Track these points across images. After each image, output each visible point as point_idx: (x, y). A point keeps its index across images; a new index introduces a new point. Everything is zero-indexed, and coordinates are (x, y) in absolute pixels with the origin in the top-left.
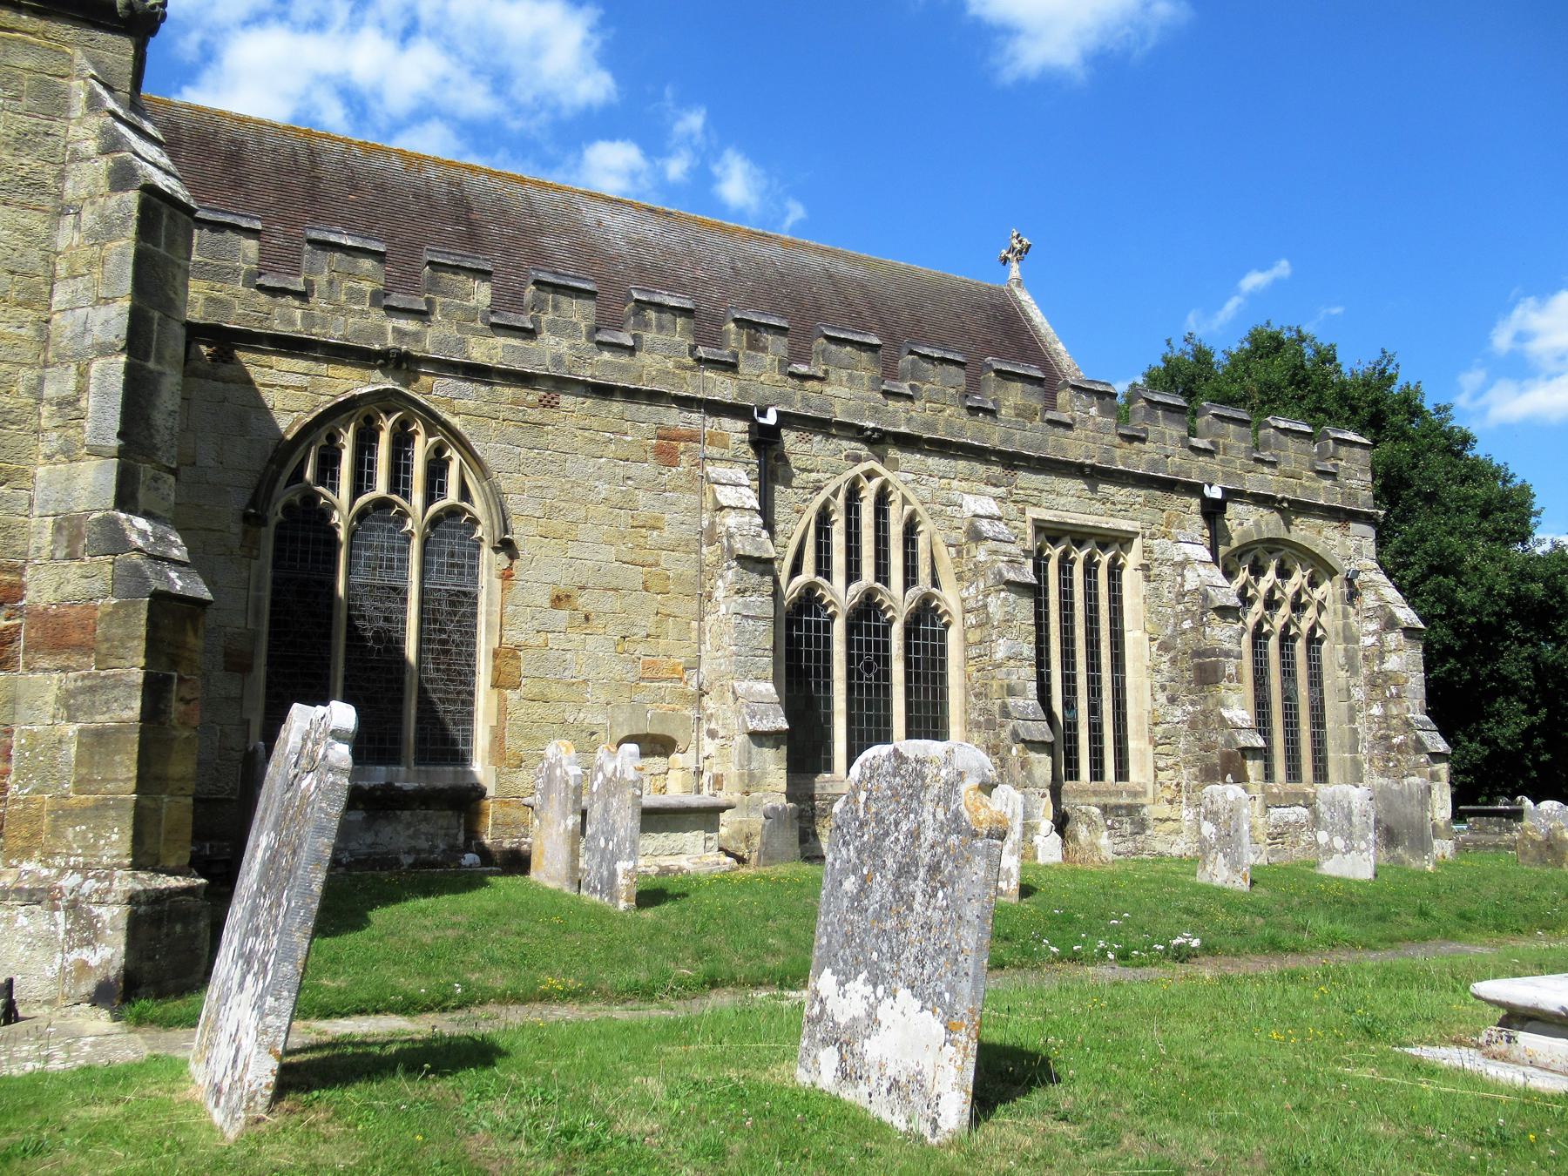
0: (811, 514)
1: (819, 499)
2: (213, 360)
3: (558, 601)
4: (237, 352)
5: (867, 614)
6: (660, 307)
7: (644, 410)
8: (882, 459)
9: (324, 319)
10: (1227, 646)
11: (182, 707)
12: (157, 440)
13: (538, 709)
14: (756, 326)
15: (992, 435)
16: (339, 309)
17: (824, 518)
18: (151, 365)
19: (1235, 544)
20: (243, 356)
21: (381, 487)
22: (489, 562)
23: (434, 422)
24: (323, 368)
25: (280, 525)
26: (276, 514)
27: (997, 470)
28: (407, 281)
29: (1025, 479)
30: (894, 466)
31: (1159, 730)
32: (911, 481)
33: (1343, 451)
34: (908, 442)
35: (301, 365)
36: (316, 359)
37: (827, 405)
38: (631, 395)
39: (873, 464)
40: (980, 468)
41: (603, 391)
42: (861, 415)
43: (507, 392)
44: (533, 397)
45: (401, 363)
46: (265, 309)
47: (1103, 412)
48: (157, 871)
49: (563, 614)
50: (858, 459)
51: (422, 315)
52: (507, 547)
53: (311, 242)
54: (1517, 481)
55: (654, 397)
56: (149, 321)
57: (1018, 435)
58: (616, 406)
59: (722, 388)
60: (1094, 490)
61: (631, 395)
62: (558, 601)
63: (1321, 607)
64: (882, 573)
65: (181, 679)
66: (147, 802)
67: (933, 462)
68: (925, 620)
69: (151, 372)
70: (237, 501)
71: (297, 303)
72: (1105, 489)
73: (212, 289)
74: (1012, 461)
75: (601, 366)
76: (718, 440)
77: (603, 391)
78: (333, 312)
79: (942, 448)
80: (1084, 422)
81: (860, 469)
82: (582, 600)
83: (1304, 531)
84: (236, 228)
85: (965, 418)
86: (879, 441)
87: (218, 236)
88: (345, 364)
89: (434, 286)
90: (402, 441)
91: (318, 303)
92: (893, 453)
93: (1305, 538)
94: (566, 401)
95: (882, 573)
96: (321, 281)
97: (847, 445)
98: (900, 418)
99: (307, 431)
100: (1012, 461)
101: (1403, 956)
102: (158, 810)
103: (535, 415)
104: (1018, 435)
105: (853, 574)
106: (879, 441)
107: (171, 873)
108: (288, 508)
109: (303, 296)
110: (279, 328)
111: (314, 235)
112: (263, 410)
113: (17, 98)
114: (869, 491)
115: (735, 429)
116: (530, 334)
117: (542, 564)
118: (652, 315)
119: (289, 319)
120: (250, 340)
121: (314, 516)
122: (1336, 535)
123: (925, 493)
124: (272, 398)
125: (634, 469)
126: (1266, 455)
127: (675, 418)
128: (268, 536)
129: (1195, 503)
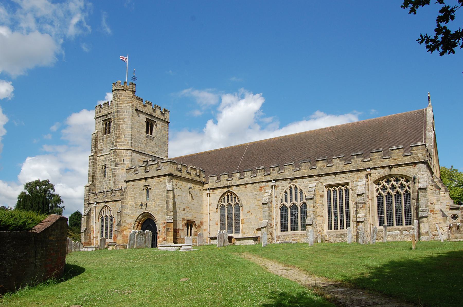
7: (257, 184)
15: (315, 172)
21: (294, 201)
28: (254, 173)
29: (323, 178)
32: (300, 184)
33: (414, 148)
34: (322, 175)
37: (417, 158)
42: (290, 176)
43: (241, 187)
45: (228, 187)
50: (290, 183)
54: (61, 205)
55: (258, 182)
64: (296, 200)
67: (304, 180)
79: (305, 177)
86: (292, 180)
90: (231, 195)
95: (296, 200)
98: (298, 174)
103: (245, 189)
105: (291, 200)
122: (412, 169)
125: (257, 193)
127: (262, 184)
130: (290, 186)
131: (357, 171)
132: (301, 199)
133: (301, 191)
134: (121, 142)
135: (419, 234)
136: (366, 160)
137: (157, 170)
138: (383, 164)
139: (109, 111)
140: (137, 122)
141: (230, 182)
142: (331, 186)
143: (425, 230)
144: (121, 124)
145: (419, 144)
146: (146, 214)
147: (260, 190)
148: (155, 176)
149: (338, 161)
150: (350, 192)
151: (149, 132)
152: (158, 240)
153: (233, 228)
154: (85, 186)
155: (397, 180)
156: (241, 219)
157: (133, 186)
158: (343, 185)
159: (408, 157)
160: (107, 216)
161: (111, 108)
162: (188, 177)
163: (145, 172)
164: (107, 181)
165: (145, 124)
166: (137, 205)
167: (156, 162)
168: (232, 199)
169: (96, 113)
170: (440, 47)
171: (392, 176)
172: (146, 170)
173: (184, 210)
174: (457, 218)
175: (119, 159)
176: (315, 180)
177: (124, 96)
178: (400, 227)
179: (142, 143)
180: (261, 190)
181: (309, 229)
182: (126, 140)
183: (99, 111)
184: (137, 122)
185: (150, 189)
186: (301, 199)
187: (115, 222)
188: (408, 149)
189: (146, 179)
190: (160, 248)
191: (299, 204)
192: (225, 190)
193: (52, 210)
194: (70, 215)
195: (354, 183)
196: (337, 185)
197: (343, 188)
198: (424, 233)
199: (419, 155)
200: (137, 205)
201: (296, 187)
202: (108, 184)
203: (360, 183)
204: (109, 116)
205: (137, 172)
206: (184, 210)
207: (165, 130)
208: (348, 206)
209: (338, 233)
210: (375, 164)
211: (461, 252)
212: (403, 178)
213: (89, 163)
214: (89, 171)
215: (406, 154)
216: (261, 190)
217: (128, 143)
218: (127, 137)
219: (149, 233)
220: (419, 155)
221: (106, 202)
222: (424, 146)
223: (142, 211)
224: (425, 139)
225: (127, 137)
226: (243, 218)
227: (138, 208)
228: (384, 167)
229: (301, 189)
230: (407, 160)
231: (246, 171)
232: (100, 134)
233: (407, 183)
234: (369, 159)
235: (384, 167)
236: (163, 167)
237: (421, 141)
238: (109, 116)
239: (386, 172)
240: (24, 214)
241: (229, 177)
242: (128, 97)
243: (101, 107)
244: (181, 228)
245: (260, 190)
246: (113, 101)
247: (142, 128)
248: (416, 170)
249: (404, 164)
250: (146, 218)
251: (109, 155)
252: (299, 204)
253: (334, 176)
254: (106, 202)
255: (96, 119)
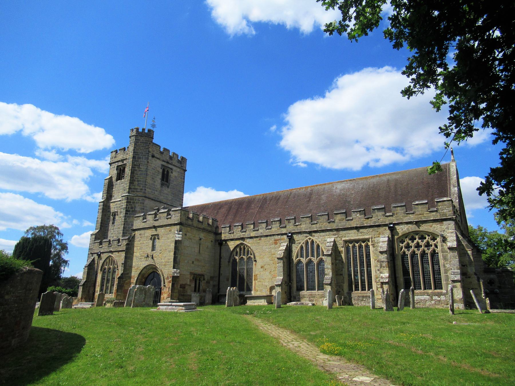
0: (299, 248)
1: (300, 245)
3: (262, 267)
5: (423, 254)
6: (275, 221)
7: (272, 237)
8: (311, 236)
10: (383, 260)
13: (260, 283)
14: (289, 219)
15: (334, 226)
17: (302, 247)
19: (400, 235)
22: (254, 263)
23: (247, 246)
27: (335, 232)
29: (342, 233)
30: (314, 236)
31: (378, 279)
32: (317, 238)
33: (439, 204)
35: (233, 242)
38: (270, 235)
39: (310, 237)
40: (331, 233)
41: (267, 236)
44: (258, 239)
45: (243, 239)
47: (360, 215)
49: (262, 269)
50: (307, 237)
51: (245, 232)
52: (255, 261)
55: (273, 235)
57: (340, 224)
58: (269, 238)
59: (284, 231)
60: (358, 231)
61: (270, 235)
62: (262, 267)
63: (436, 246)
67: (322, 234)
68: (434, 254)
70: (227, 260)
72: (361, 230)
74: (338, 230)
75: (267, 232)
76: (284, 239)
77: (267, 236)
79: (323, 231)
80: (355, 218)
81: (307, 238)
82: (265, 267)
83: (424, 228)
85: (328, 224)
86: (310, 233)
89: (247, 227)
90: (244, 249)
91: (235, 233)
92: (313, 234)
93: (425, 229)
94: (262, 238)
97: (305, 235)
98: (315, 228)
99: (233, 250)
100: (338, 230)
103: (259, 241)
104: (340, 224)
105: (307, 256)
106: (310, 233)
109: (233, 233)
114: (309, 241)
115: (285, 236)
116: (258, 230)
117: (260, 262)
118: (274, 223)
119: (232, 236)
120: (228, 240)
121: (235, 260)
123: (320, 240)
126: (331, 220)
127: (277, 237)
129: (387, 228)
130: (307, 240)
131: (379, 226)
132: (318, 255)
133: (318, 246)
135: (453, 301)
136: (388, 214)
137: (167, 219)
138: (406, 220)
139: (125, 157)
140: (153, 169)
141: (244, 233)
142: (351, 241)
143: (458, 296)
144: (136, 170)
145: (445, 199)
147: (275, 243)
149: (358, 215)
150: (371, 249)
151: (165, 180)
152: (162, 296)
155: (422, 238)
156: (254, 274)
157: (140, 235)
158: (364, 241)
159: (434, 213)
160: (110, 269)
161: (127, 154)
162: (200, 226)
165: (161, 171)
166: (142, 256)
167: (166, 210)
168: (244, 252)
170: (481, 117)
171: (416, 233)
173: (193, 262)
174: (493, 283)
175: (130, 206)
176: (333, 235)
178: (430, 291)
179: (156, 191)
180: (276, 243)
181: (327, 289)
182: (140, 186)
184: (153, 169)
186: (318, 255)
187: (118, 275)
188: (431, 205)
189: (155, 227)
190: (161, 307)
191: (315, 260)
192: (238, 242)
194: (15, 243)
195: (376, 239)
196: (357, 241)
197: (363, 244)
198: (458, 299)
199: (445, 211)
200: (142, 256)
201: (312, 242)
202: (116, 232)
203: (381, 239)
204: (125, 162)
205: (145, 220)
206: (193, 262)
207: (181, 178)
208: (369, 265)
209: (360, 295)
210: (398, 219)
211: (3, 101)
212: (429, 236)
213: (99, 209)
215: (431, 209)
216: (276, 243)
220: (445, 211)
221: (111, 252)
222: (450, 202)
223: (147, 263)
224: (450, 195)
226: (256, 273)
228: (407, 223)
229: (318, 244)
230: (433, 216)
231: (261, 223)
232: (114, 179)
233: (434, 241)
234: (391, 214)
235: (407, 223)
237: (447, 196)
238: (125, 162)
239: (413, 228)
240: (19, 262)
242: (146, 143)
244: (188, 283)
245: (275, 243)
248: (443, 227)
249: (430, 220)
250: (151, 271)
251: (120, 202)
252: (315, 260)
253: (355, 231)
254: (111, 252)
255: (110, 164)
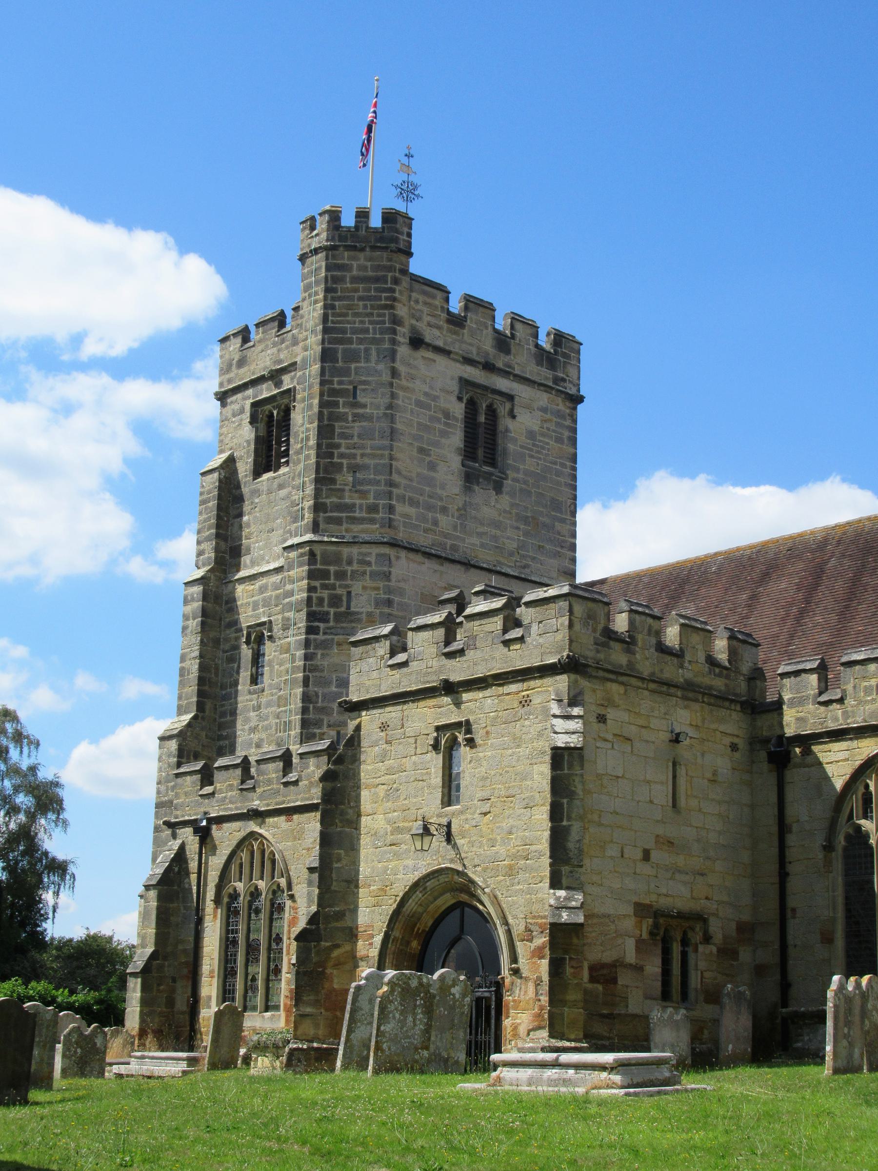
2: (803, 755)
4: (813, 747)
9: (853, 712)
11: (572, 970)
12: (571, 854)
16: (860, 702)
18: (565, 823)
20: (816, 748)
24: (855, 743)
25: (845, 849)
26: (841, 841)
35: (844, 745)
36: (851, 739)
46: (823, 716)
48: (562, 1039)
53: (843, 664)
56: (562, 805)
65: (571, 959)
66: (554, 1010)
69: (564, 826)
70: (820, 840)
71: (838, 706)
73: (798, 712)
78: (858, 704)
84: (805, 671)
87: (798, 679)
88: (866, 738)
91: (850, 702)
96: (849, 687)
99: (849, 786)
101: (862, 1055)
102: (562, 1015)
107: (569, 1040)
108: (848, 837)
109: (841, 701)
110: (832, 726)
111: (845, 659)
112: (827, 779)
113: (537, 717)
119: (835, 718)
124: (830, 770)
128: (838, 856)
134: (340, 507)
137: (507, 643)
140: (419, 404)
144: (342, 418)
146: (443, 879)
148: (497, 677)
151: (480, 453)
153: (830, 1023)
154: (160, 733)
160: (255, 894)
161: (295, 342)
163: (450, 655)
164: (269, 704)
167: (498, 603)
169: (226, 368)
172: (447, 643)
173: (646, 856)
175: (325, 594)
177: (354, 280)
179: (444, 510)
182: (363, 494)
183: (237, 358)
185: (471, 743)
189: (450, 688)
190: (506, 1073)
193: (201, 820)
202: (273, 721)
204: (287, 382)
206: (646, 856)
213: (186, 617)
214: (183, 659)
217: (373, 509)
218: (370, 482)
219: (455, 983)
225: (370, 482)
227: (407, 844)
232: (244, 468)
236: (534, 628)
238: (287, 382)
241: (30, 812)
242: (377, 280)
243: (246, 339)
244: (631, 956)
246: (305, 305)
247: (444, 434)
251: (276, 578)
254: (256, 815)
255: (222, 397)
